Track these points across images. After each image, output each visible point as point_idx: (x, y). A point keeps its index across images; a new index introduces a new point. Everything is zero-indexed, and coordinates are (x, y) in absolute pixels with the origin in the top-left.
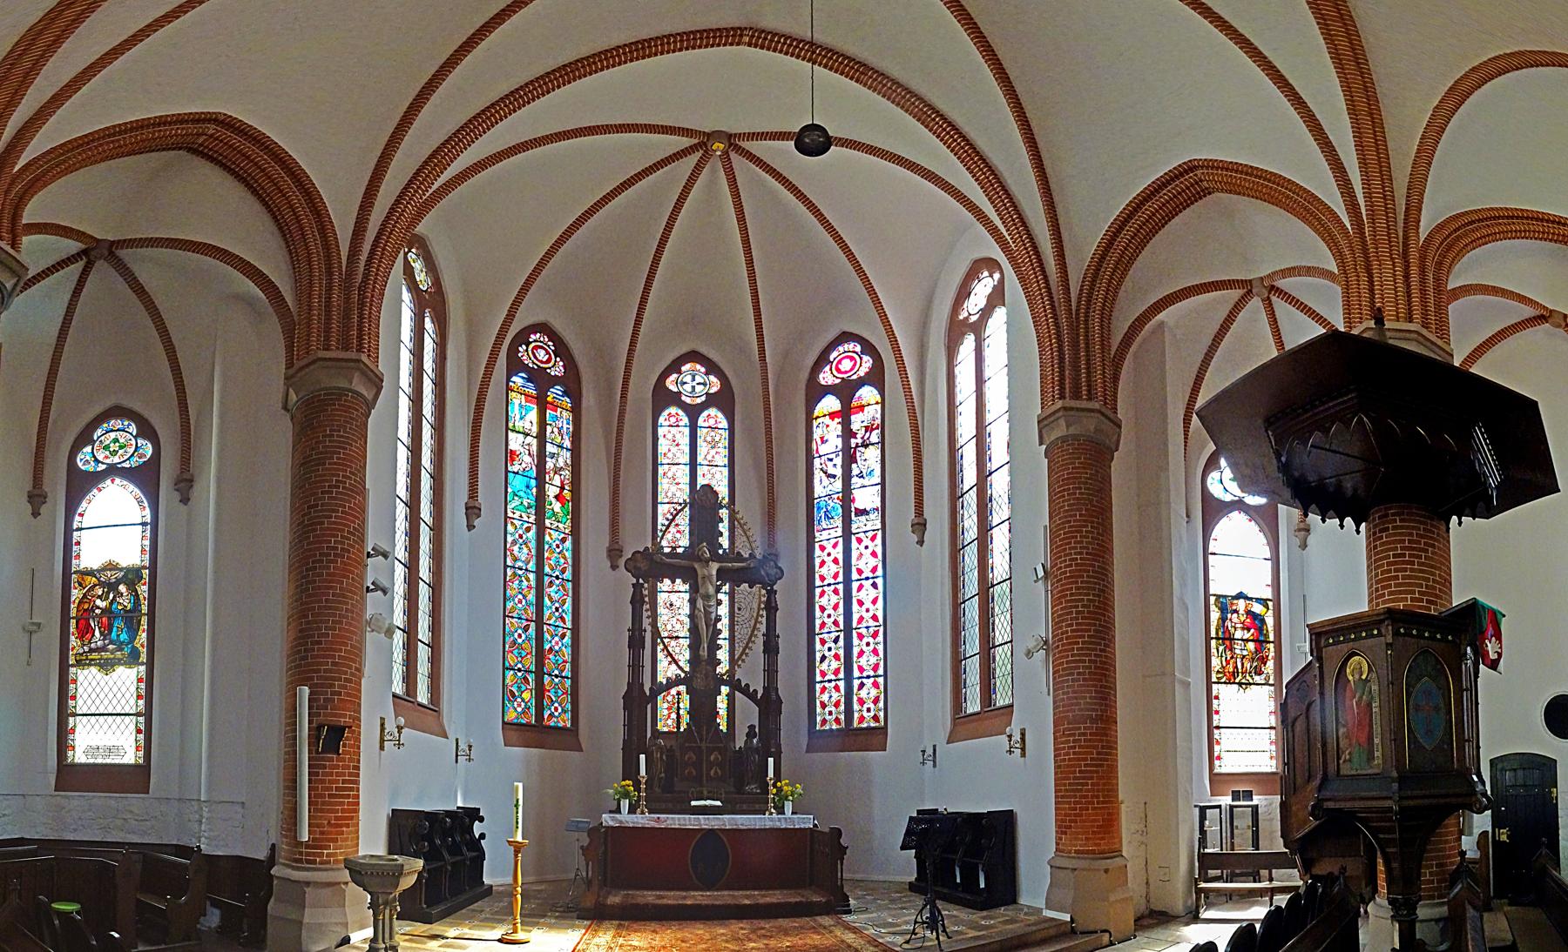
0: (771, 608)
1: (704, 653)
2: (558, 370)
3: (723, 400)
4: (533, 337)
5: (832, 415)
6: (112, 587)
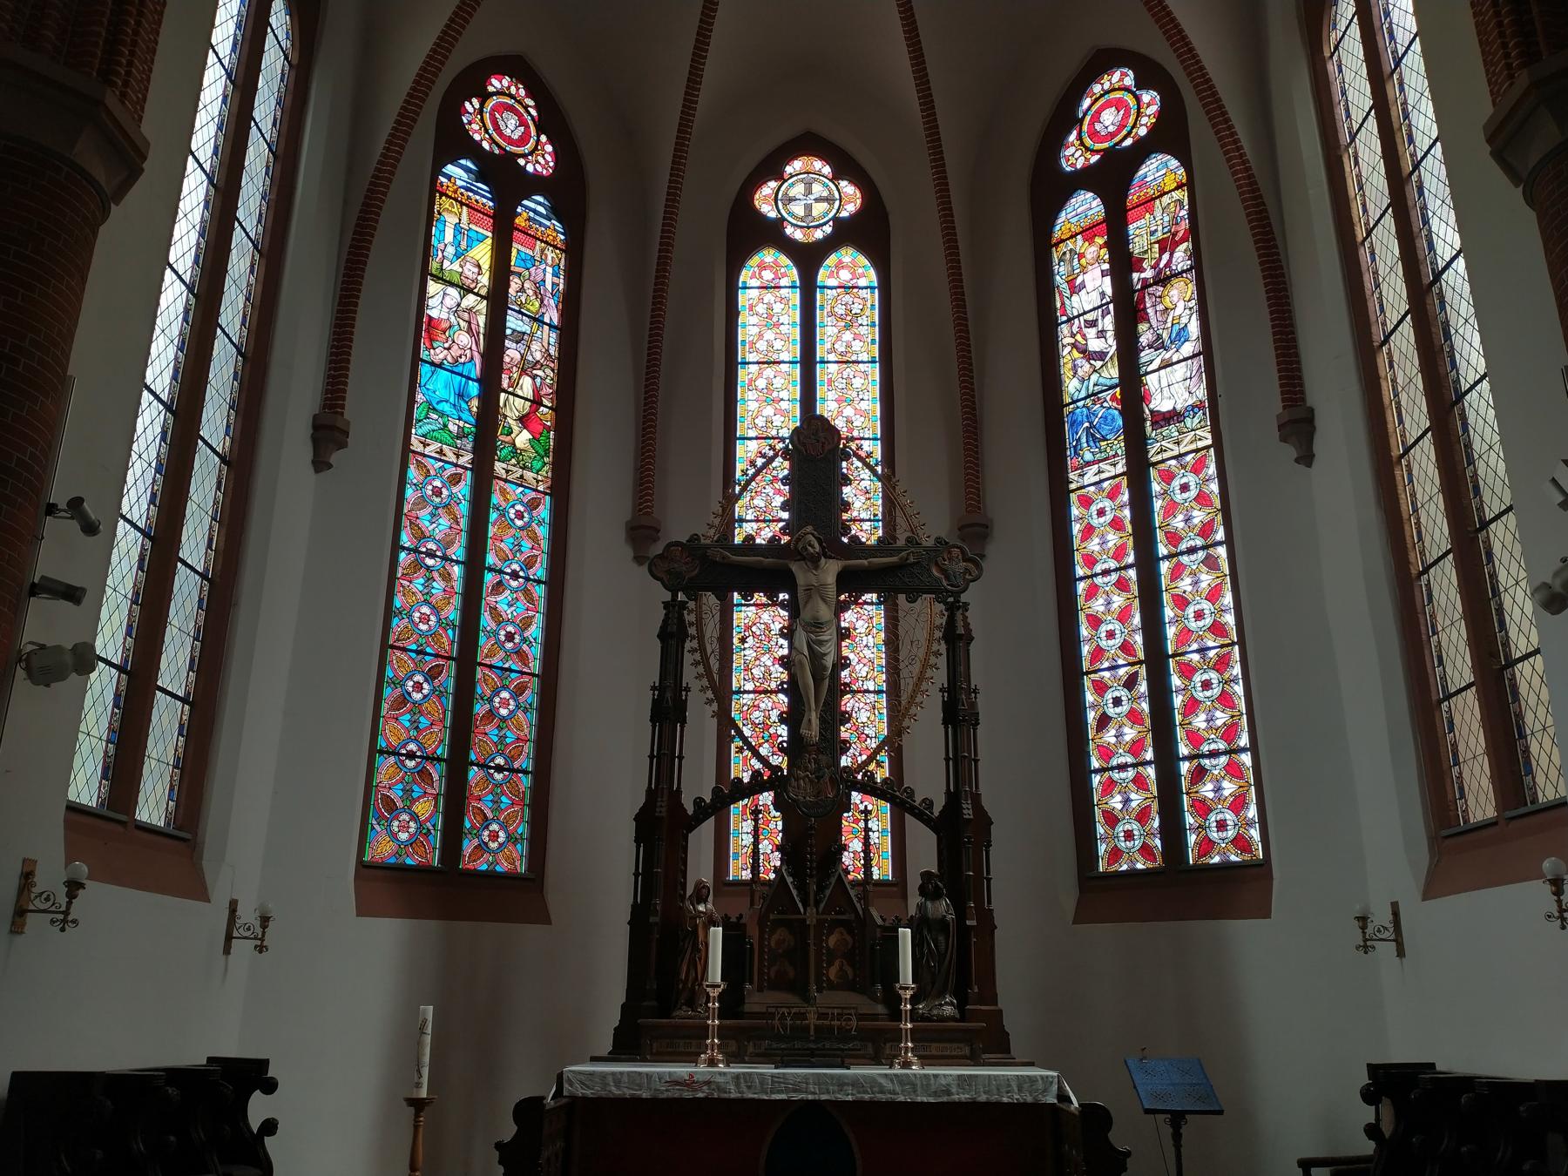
0: (956, 639)
1: (812, 728)
2: (541, 161)
4: (495, 84)
5: (1088, 233)
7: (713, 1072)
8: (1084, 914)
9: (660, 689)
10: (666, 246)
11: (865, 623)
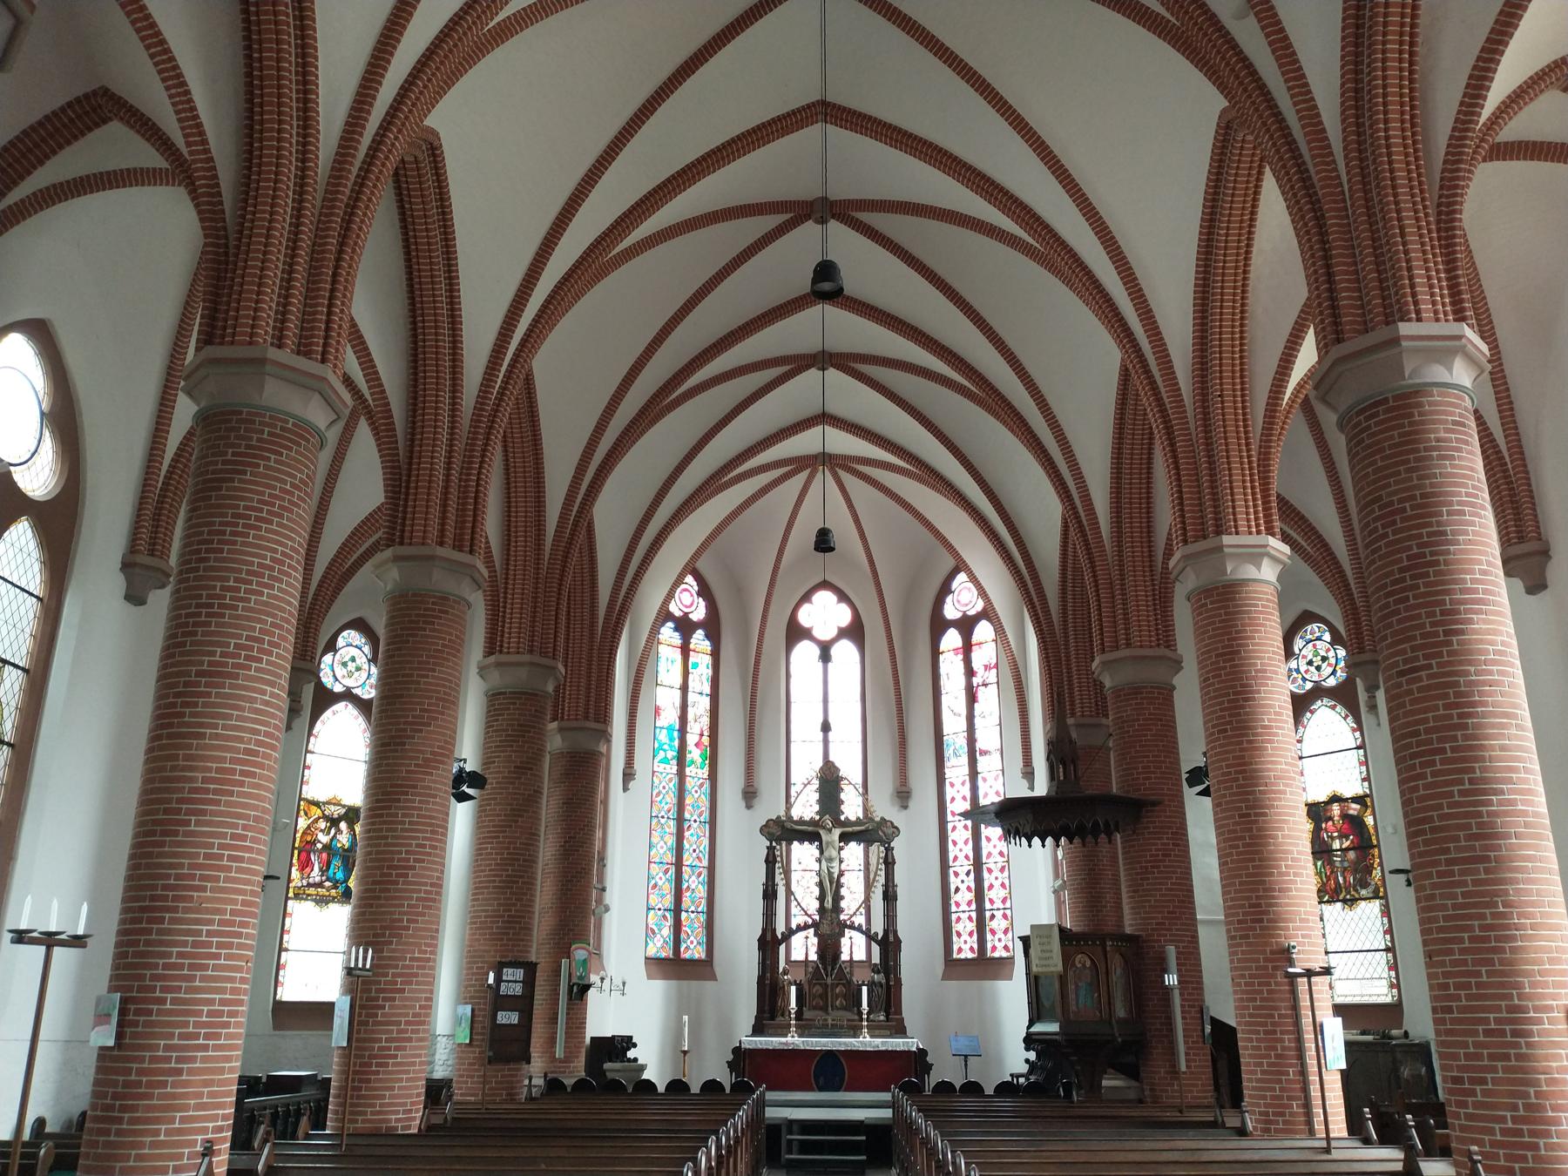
0: (889, 863)
1: (829, 904)
3: (855, 632)
6: (334, 822)
7: (793, 1040)
8: (947, 976)
9: (766, 885)
10: (757, 663)
11: (854, 853)
